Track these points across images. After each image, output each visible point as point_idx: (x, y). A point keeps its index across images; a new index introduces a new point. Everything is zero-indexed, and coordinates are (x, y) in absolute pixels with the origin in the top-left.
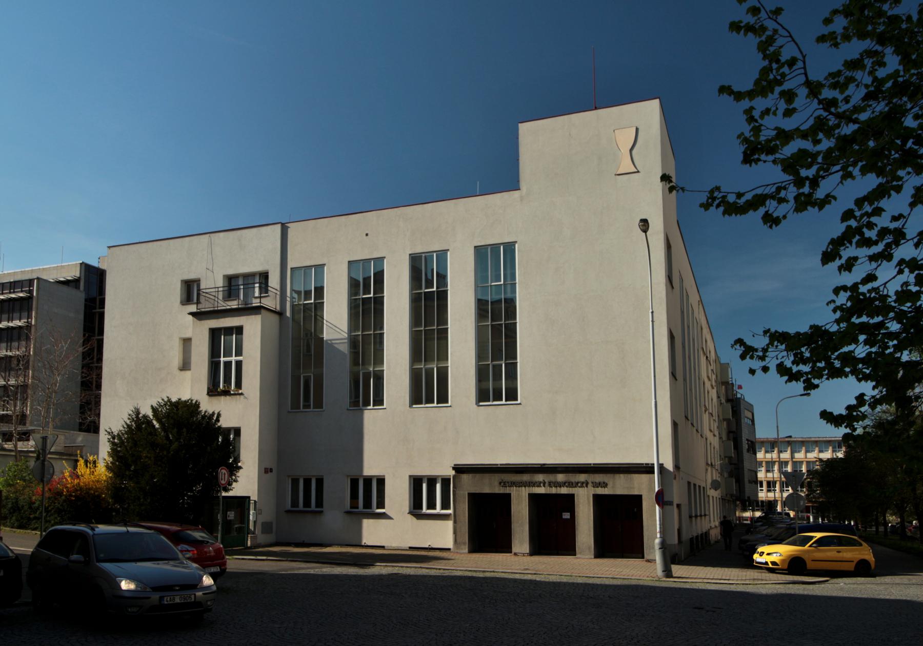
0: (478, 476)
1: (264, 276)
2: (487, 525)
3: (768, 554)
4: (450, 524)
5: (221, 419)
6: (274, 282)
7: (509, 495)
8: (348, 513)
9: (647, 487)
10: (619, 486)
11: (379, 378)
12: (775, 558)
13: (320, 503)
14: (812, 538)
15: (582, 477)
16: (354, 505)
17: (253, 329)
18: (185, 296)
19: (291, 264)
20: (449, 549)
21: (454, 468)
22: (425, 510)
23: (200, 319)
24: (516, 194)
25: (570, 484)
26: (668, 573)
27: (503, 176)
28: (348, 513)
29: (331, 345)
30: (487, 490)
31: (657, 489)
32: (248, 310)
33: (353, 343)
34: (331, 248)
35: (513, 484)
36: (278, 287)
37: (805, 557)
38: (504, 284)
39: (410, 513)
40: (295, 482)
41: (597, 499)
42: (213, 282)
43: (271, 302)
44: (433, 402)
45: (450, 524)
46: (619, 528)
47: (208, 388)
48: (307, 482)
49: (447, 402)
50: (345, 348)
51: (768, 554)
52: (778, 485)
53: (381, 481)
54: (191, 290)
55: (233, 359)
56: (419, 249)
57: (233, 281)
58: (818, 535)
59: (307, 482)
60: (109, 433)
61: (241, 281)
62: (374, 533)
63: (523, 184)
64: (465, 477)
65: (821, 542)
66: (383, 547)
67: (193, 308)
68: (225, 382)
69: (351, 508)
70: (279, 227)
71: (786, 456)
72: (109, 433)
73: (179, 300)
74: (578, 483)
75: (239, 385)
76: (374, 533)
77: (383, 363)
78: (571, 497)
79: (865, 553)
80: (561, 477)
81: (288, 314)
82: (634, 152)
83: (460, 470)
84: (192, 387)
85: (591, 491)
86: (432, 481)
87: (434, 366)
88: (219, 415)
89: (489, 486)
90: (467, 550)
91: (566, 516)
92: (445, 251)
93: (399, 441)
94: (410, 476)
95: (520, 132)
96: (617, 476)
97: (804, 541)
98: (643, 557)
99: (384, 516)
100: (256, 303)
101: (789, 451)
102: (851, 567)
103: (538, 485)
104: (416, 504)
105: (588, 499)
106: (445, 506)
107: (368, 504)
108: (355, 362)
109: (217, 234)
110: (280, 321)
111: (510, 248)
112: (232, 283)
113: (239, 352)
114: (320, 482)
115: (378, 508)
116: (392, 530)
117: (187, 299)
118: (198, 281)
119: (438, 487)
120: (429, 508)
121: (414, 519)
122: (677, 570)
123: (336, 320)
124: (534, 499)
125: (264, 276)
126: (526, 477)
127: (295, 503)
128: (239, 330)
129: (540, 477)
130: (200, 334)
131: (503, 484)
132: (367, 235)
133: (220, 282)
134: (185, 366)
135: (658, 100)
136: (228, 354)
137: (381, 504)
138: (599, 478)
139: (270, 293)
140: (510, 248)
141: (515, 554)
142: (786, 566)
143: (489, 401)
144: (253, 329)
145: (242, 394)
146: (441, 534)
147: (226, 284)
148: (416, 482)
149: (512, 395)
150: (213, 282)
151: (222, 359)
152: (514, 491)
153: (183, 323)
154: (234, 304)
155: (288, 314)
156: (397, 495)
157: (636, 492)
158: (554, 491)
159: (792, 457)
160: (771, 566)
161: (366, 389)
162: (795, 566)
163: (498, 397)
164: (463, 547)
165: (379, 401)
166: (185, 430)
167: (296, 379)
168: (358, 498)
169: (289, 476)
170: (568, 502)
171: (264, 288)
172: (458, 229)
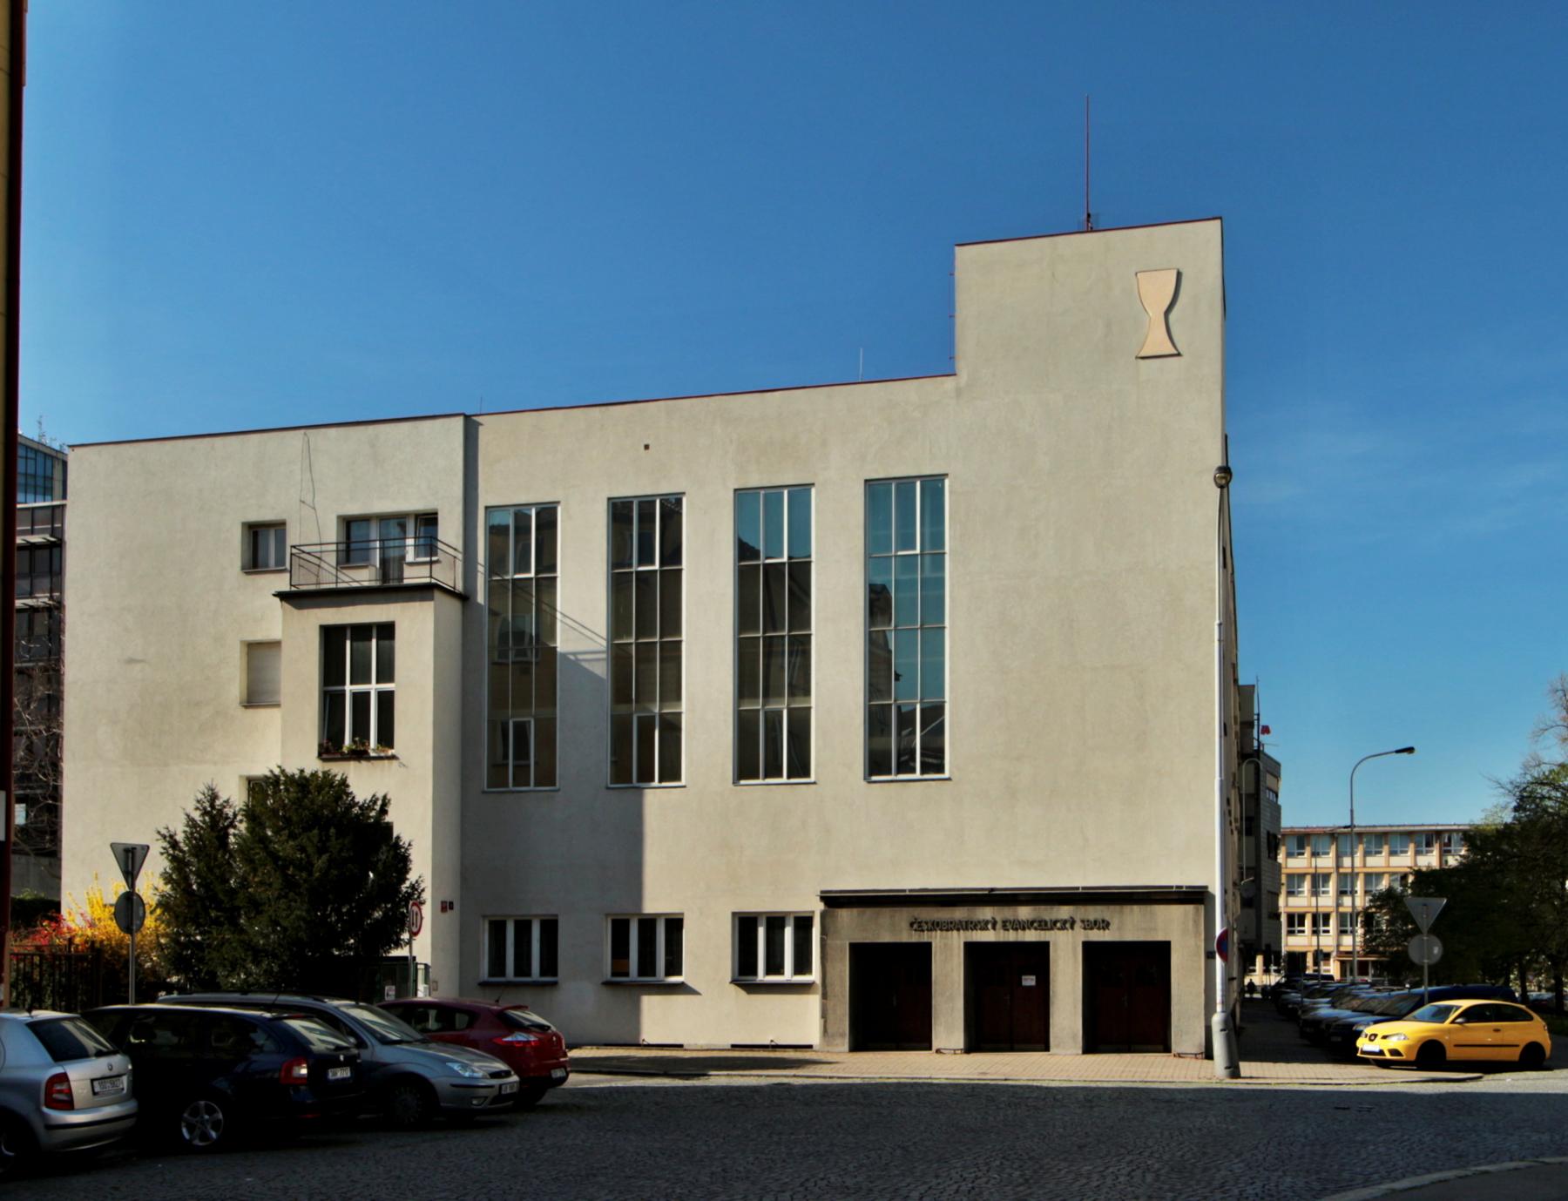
0: (869, 912)
1: (428, 520)
2: (886, 999)
3: (1385, 1037)
4: (813, 1001)
5: (390, 809)
6: (450, 531)
7: (929, 945)
8: (607, 984)
9: (1172, 926)
10: (1129, 926)
11: (672, 727)
12: (1386, 1046)
13: (550, 966)
14: (1449, 1009)
15: (1064, 912)
16: (620, 967)
17: (419, 634)
18: (249, 555)
19: (485, 498)
20: (810, 1047)
21: (823, 899)
22: (762, 976)
23: (299, 607)
24: (949, 383)
25: (1043, 925)
26: (1234, 1072)
27: (921, 345)
28: (607, 984)
29: (574, 663)
30: (886, 937)
31: (1218, 931)
32: (391, 589)
33: (618, 656)
34: (572, 468)
35: (936, 926)
36: (459, 545)
37: (1445, 1039)
38: (922, 554)
39: (734, 981)
40: (497, 929)
41: (1092, 952)
42: (315, 530)
43: (449, 574)
44: (781, 775)
45: (813, 1001)
46: (1129, 997)
47: (320, 746)
48: (523, 928)
49: (807, 774)
50: (601, 669)
51: (1385, 1037)
52: (1333, 921)
53: (675, 925)
54: (261, 544)
55: (373, 687)
56: (755, 479)
57: (354, 527)
58: (1465, 1004)
59: (523, 928)
60: (164, 837)
61: (374, 533)
62: (664, 1022)
63: (963, 366)
64: (845, 915)
65: (1470, 1015)
66: (680, 1046)
67: (282, 583)
68: (354, 733)
69: (614, 974)
70: (459, 423)
71: (1326, 862)
72: (164, 837)
73: (238, 564)
74: (1055, 922)
75: (386, 738)
76: (664, 1022)
77: (679, 698)
78: (1044, 947)
79: (1535, 1030)
80: (1024, 912)
81: (481, 598)
82: (1172, 317)
83: (833, 901)
84: (283, 743)
85: (1080, 936)
86: (775, 923)
87: (783, 706)
88: (385, 802)
89: (892, 930)
90: (846, 1047)
91: (1029, 981)
92: (807, 487)
93: (705, 846)
94: (734, 914)
95: (958, 263)
96: (1127, 909)
97: (1441, 1015)
98: (1167, 1049)
99: (681, 989)
100: (414, 575)
101: (1332, 854)
102: (1514, 1055)
103: (983, 926)
104: (745, 965)
105: (1074, 949)
106: (802, 965)
107: (647, 966)
108: (621, 692)
109: (323, 430)
110: (464, 613)
111: (934, 485)
112: (353, 532)
113: (386, 673)
114: (550, 928)
115: (668, 974)
116: (699, 1016)
117: (254, 563)
118: (279, 527)
119: (789, 933)
120: (769, 972)
121: (742, 993)
122: (1246, 1068)
123: (581, 613)
124: (973, 952)
125: (428, 520)
126: (960, 913)
127: (497, 965)
128: (386, 631)
129: (986, 913)
130: (299, 638)
131: (917, 925)
132: (647, 447)
133: (332, 533)
134: (257, 696)
135: (1218, 222)
136: (361, 676)
137: (674, 966)
138: (1094, 912)
139: (440, 556)
140: (934, 485)
141: (1179, 1055)
142: (1413, 1057)
143: (889, 773)
144: (419, 634)
145: (393, 757)
146: (802, 1020)
147: (343, 539)
148: (745, 925)
149: (934, 762)
150: (315, 530)
151: (349, 688)
152: (937, 939)
153: (260, 608)
154: (364, 577)
155: (481, 598)
156: (707, 951)
157: (1160, 937)
158: (1012, 936)
159: (1338, 866)
160: (1388, 1056)
161: (644, 747)
162: (1429, 1055)
163: (905, 766)
164: (838, 1041)
165: (672, 771)
166: (332, 830)
167: (498, 729)
168: (626, 955)
169: (484, 917)
170: (1038, 957)
171: (429, 546)
172: (835, 444)
